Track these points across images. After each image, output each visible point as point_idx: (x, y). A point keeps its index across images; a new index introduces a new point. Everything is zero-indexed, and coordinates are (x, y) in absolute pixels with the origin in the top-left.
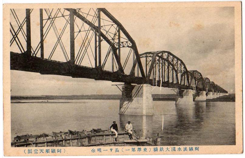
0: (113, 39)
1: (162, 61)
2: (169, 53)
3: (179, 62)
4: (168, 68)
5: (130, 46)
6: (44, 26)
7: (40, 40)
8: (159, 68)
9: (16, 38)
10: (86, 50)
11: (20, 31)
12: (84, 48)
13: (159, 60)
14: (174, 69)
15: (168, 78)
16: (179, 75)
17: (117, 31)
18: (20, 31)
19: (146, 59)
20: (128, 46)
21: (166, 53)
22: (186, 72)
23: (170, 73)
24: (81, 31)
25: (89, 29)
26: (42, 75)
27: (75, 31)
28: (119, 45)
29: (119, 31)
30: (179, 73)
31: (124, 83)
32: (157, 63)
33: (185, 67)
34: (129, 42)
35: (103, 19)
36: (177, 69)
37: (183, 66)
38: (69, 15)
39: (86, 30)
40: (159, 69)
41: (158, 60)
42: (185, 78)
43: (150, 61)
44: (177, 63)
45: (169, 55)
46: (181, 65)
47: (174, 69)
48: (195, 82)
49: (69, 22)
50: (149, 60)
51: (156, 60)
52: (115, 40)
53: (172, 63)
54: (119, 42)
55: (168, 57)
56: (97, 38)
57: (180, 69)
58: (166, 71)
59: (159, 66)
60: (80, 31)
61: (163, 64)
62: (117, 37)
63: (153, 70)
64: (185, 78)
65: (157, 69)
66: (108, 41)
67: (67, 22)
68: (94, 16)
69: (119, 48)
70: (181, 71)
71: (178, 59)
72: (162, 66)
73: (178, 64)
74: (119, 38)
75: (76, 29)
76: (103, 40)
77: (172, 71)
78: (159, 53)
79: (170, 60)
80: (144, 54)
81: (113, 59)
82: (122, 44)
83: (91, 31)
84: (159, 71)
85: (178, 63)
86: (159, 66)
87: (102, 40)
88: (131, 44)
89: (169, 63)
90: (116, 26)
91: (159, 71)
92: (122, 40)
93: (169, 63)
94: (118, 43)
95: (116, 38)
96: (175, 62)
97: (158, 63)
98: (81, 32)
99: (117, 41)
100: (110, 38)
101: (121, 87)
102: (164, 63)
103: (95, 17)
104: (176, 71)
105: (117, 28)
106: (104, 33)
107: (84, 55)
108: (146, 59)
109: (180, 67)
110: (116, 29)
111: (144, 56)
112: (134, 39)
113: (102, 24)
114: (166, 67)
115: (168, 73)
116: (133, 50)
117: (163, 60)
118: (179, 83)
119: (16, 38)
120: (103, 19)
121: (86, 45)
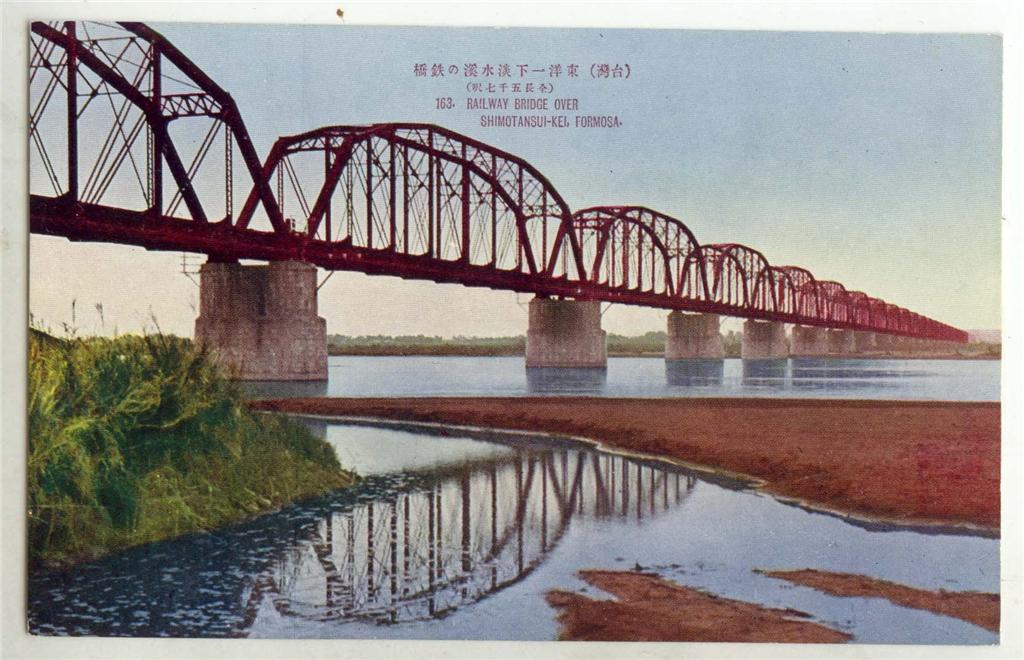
5: (558, 214)
6: (82, 112)
7: (79, 122)
11: (125, 154)
15: (729, 296)
18: (125, 154)
20: (208, 113)
22: (697, 253)
26: (370, 277)
33: (692, 238)
42: (764, 289)
46: (758, 263)
48: (791, 298)
55: (640, 217)
64: (764, 289)
67: (55, 79)
82: (168, 105)
98: (98, 97)
104: (664, 250)
107: (136, 131)
118: (289, 148)
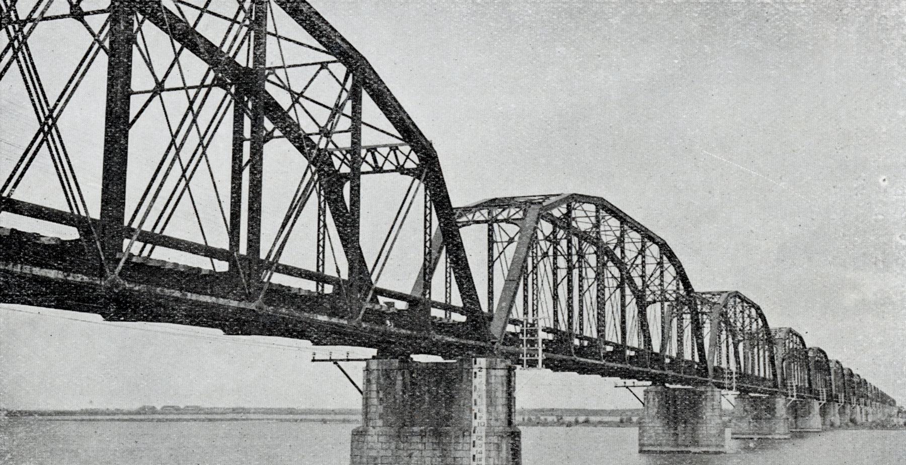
0: (326, 133)
1: (569, 242)
2: (603, 206)
3: (654, 250)
4: (599, 276)
5: (409, 165)
8: (555, 280)
9: (206, 84)
10: (186, 177)
12: (176, 171)
13: (554, 241)
14: (625, 280)
16: (654, 313)
17: (345, 95)
19: (491, 230)
21: (587, 206)
23: (608, 307)
24: (167, 85)
25: (208, 81)
27: (135, 85)
28: (355, 166)
29: (355, 97)
30: (654, 302)
31: (374, 352)
32: (545, 255)
33: (682, 277)
34: (406, 149)
35: (630, 250)
36: (644, 282)
37: (672, 270)
38: (105, 7)
39: (188, 85)
40: (556, 286)
41: (547, 238)
43: (511, 241)
44: (642, 252)
45: (603, 213)
47: (625, 280)
48: (731, 348)
49: (107, 44)
50: (506, 238)
51: (540, 236)
52: (335, 137)
53: (618, 252)
54: (353, 143)
55: (597, 225)
56: (247, 122)
57: (657, 282)
58: (587, 294)
59: (555, 269)
60: (159, 88)
61: (575, 258)
62: (344, 123)
63: (526, 285)
65: (546, 283)
66: (301, 142)
68: (234, 21)
69: (355, 176)
70: (663, 291)
71: (648, 236)
72: (570, 269)
73: (649, 260)
74: (355, 131)
75: (141, 79)
76: (277, 133)
77: (618, 291)
78: (553, 206)
79: (609, 237)
80: (479, 207)
81: (322, 226)
82: (369, 158)
83: (214, 89)
84: (555, 297)
85: (647, 252)
86: (555, 269)
87: (270, 136)
88: (413, 156)
89: (604, 252)
90: (340, 70)
91: (555, 297)
92: (368, 137)
93: (604, 252)
94: (348, 152)
95: (338, 128)
96: (631, 250)
97: (551, 253)
99: (344, 141)
100: (307, 126)
101: (357, 371)
102: (581, 255)
103: (236, 26)
105: (346, 79)
106: (283, 100)
108: (491, 230)
109: (658, 272)
110: (343, 85)
111: (478, 216)
112: (429, 132)
113: (272, 58)
114: (591, 274)
115: (601, 305)
116: (422, 186)
117: (575, 240)
119: (206, 84)
120: (630, 250)
121: (185, 155)
